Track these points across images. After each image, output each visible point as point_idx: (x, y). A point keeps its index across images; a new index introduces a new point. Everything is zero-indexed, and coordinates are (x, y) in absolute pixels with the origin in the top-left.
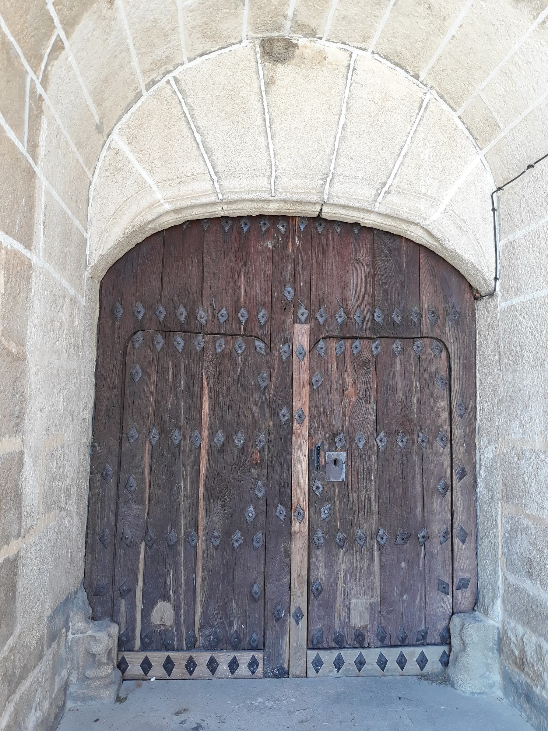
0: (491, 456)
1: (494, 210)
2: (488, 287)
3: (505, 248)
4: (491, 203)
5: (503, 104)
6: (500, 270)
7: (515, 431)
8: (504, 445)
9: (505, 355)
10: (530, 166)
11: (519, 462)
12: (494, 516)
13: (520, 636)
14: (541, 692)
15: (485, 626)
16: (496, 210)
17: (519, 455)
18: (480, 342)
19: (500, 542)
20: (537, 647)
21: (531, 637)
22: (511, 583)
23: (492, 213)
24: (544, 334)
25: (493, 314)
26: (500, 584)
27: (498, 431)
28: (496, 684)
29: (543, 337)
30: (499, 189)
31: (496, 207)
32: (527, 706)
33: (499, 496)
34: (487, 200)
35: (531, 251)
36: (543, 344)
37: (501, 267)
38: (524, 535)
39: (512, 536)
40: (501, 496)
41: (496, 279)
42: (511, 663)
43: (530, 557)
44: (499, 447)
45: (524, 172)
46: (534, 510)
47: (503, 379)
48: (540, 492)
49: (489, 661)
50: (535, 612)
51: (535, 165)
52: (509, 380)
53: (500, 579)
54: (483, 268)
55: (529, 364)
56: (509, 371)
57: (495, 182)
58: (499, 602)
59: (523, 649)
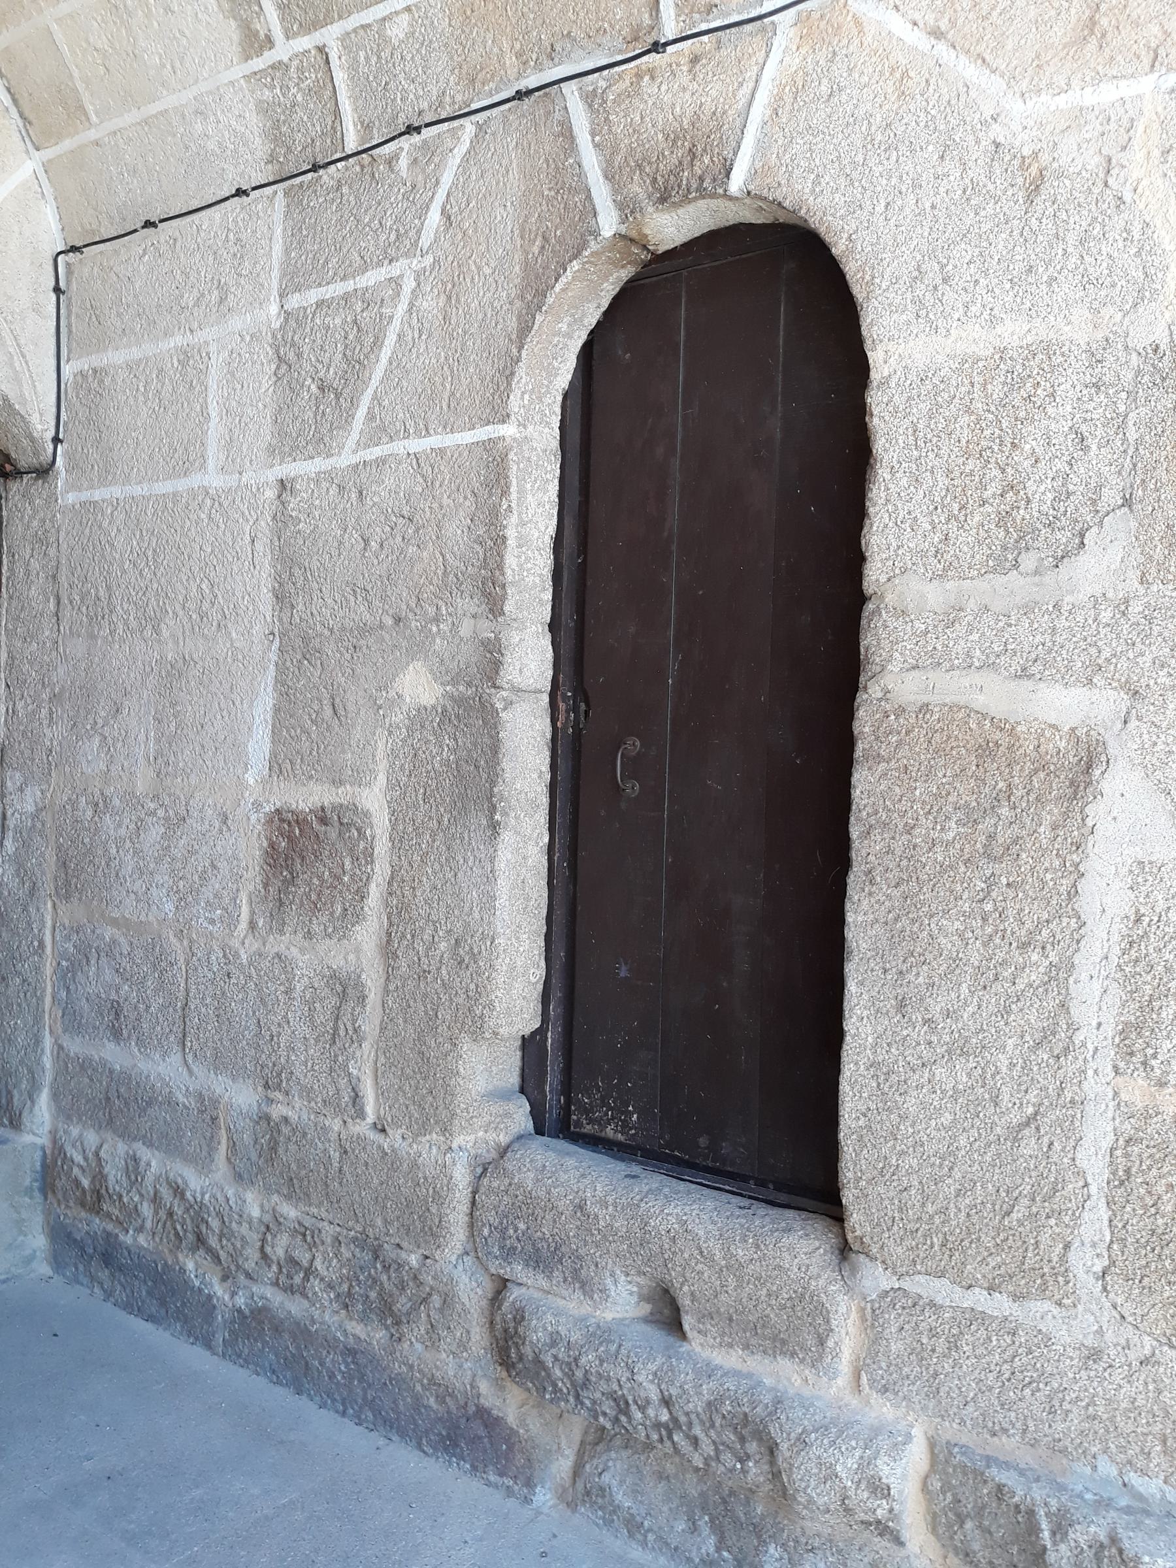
0: (30, 808)
1: (57, 290)
2: (36, 453)
3: (79, 378)
4: (52, 273)
5: (102, 70)
6: (66, 424)
7: (90, 758)
8: (62, 786)
9: (71, 602)
10: (148, 224)
11: (96, 818)
12: (36, 931)
13: (93, 1149)
14: (135, 1239)
15: (15, 1150)
16: (64, 293)
17: (97, 804)
18: (11, 570)
19: (48, 979)
20: (129, 1161)
21: (115, 1147)
22: (72, 1054)
23: (53, 297)
24: (162, 569)
25: (46, 515)
26: (47, 1061)
27: (50, 758)
28: (38, 1253)
29: (159, 575)
30: (74, 249)
31: (62, 285)
32: (104, 1275)
33: (50, 888)
34: (44, 265)
35: (141, 398)
36: (160, 590)
37: (68, 417)
38: (104, 959)
39: (77, 963)
40: (53, 888)
41: (56, 440)
42: (71, 1204)
43: (116, 998)
44: (52, 789)
45: (135, 231)
46: (129, 909)
47: (65, 651)
48: (142, 873)
49: (24, 1215)
50: (125, 1099)
51: (159, 225)
52: (79, 655)
53: (48, 1051)
54: (31, 412)
55: (126, 623)
56: (79, 636)
57: (63, 229)
58: (44, 1098)
59: (100, 1172)
